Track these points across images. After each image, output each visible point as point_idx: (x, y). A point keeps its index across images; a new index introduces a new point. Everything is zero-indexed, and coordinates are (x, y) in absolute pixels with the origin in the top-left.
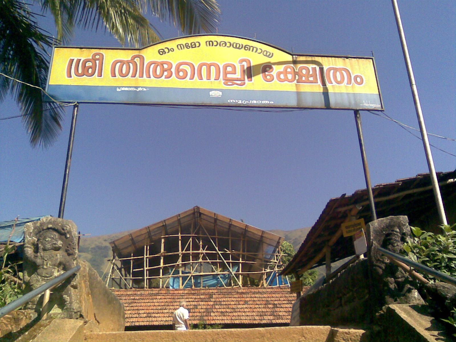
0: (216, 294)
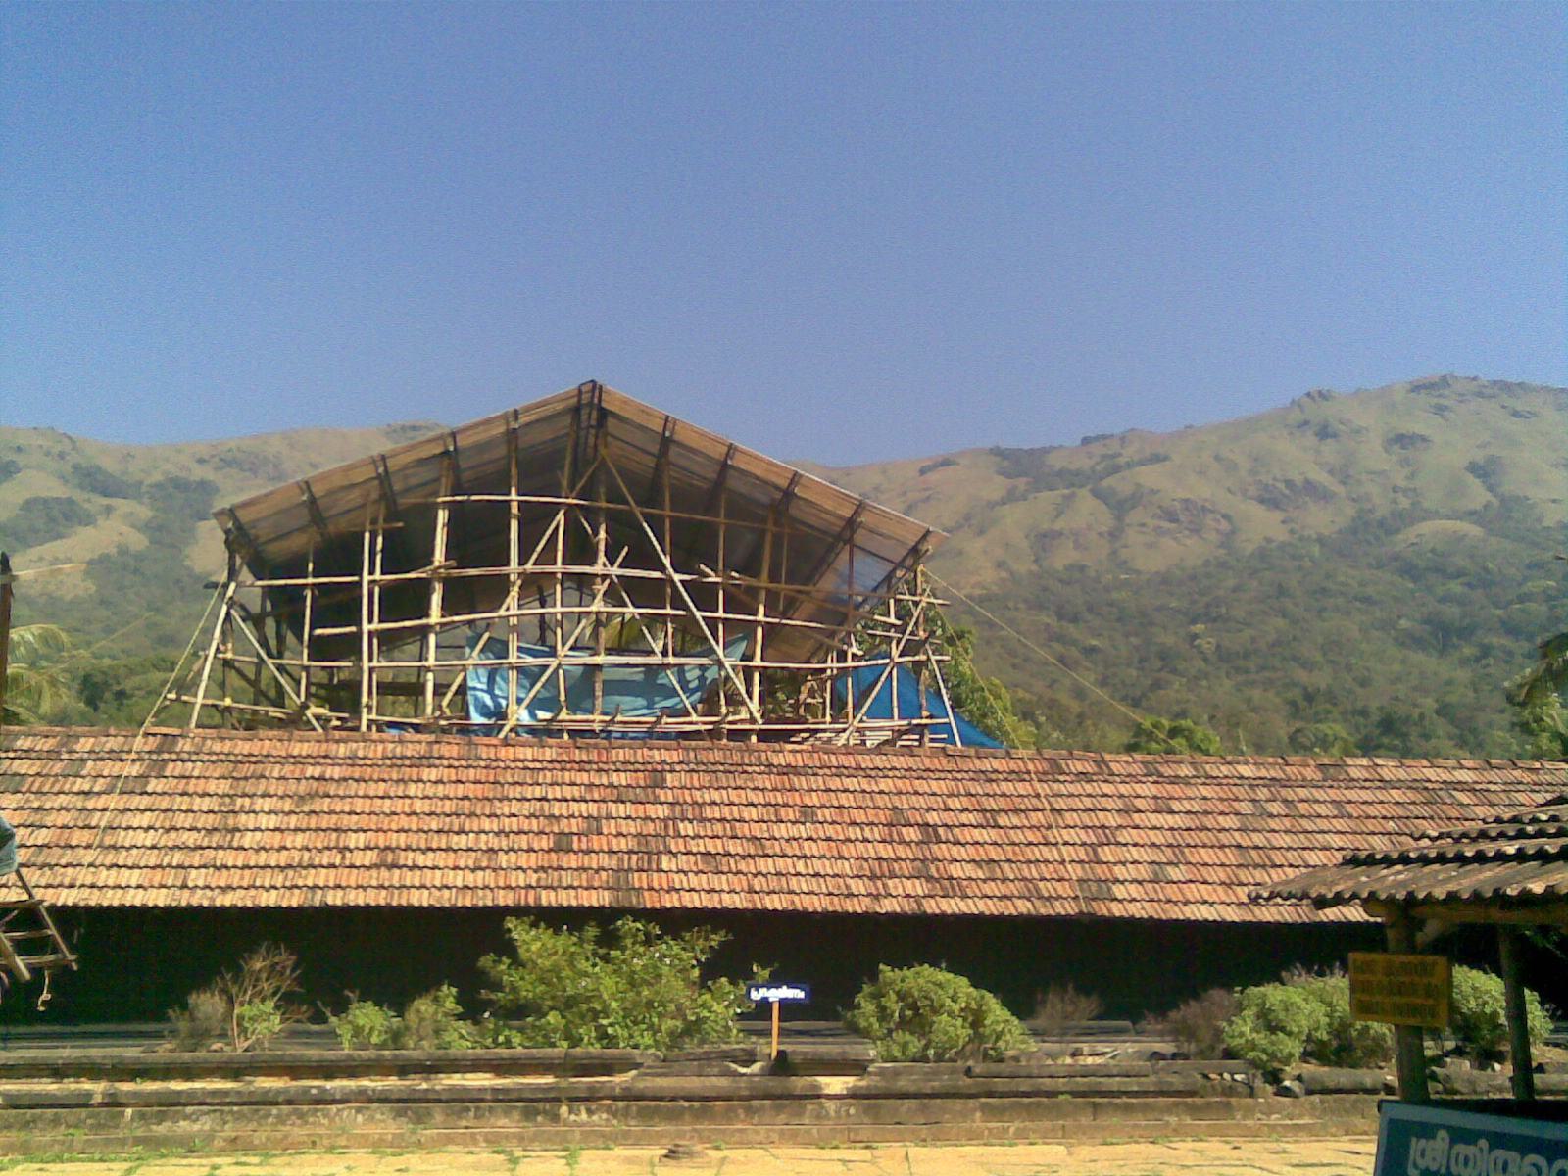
0: (678, 768)
